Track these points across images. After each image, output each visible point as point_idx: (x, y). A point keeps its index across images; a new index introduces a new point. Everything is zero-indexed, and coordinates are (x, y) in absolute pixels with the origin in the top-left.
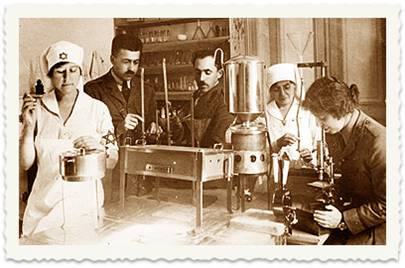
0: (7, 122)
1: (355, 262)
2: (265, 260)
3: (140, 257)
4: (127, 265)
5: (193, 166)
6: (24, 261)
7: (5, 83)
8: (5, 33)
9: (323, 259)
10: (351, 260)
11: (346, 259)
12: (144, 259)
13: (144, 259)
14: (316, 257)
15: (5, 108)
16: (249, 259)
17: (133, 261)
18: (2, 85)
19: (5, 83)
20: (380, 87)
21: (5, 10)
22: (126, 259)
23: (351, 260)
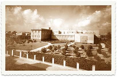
0: (2, 14)
1: (102, 75)
2: (76, 75)
3: (40, 74)
4: (36, 76)
5: (77, 57)
6: (7, 75)
7: (1, 24)
8: (1, 10)
9: (93, 75)
10: (80, 75)
11: (30, 75)
12: (41, 75)
13: (41, 75)
14: (51, 74)
15: (1, 31)
16: (72, 75)
17: (108, 75)
18: (1, 46)
19: (1, 46)
20: (28, 69)
21: (1, 3)
22: (15, 75)
23: (80, 75)
